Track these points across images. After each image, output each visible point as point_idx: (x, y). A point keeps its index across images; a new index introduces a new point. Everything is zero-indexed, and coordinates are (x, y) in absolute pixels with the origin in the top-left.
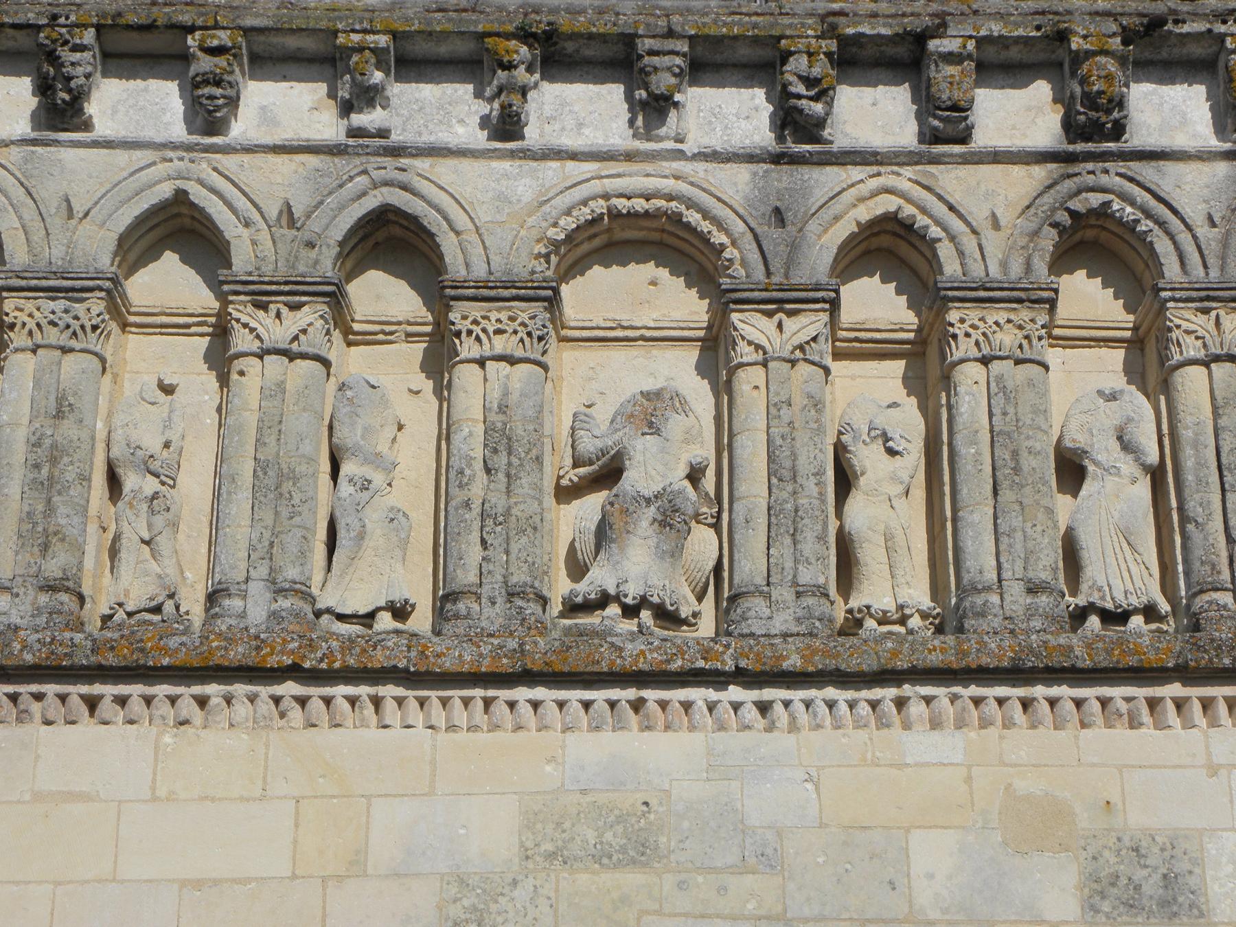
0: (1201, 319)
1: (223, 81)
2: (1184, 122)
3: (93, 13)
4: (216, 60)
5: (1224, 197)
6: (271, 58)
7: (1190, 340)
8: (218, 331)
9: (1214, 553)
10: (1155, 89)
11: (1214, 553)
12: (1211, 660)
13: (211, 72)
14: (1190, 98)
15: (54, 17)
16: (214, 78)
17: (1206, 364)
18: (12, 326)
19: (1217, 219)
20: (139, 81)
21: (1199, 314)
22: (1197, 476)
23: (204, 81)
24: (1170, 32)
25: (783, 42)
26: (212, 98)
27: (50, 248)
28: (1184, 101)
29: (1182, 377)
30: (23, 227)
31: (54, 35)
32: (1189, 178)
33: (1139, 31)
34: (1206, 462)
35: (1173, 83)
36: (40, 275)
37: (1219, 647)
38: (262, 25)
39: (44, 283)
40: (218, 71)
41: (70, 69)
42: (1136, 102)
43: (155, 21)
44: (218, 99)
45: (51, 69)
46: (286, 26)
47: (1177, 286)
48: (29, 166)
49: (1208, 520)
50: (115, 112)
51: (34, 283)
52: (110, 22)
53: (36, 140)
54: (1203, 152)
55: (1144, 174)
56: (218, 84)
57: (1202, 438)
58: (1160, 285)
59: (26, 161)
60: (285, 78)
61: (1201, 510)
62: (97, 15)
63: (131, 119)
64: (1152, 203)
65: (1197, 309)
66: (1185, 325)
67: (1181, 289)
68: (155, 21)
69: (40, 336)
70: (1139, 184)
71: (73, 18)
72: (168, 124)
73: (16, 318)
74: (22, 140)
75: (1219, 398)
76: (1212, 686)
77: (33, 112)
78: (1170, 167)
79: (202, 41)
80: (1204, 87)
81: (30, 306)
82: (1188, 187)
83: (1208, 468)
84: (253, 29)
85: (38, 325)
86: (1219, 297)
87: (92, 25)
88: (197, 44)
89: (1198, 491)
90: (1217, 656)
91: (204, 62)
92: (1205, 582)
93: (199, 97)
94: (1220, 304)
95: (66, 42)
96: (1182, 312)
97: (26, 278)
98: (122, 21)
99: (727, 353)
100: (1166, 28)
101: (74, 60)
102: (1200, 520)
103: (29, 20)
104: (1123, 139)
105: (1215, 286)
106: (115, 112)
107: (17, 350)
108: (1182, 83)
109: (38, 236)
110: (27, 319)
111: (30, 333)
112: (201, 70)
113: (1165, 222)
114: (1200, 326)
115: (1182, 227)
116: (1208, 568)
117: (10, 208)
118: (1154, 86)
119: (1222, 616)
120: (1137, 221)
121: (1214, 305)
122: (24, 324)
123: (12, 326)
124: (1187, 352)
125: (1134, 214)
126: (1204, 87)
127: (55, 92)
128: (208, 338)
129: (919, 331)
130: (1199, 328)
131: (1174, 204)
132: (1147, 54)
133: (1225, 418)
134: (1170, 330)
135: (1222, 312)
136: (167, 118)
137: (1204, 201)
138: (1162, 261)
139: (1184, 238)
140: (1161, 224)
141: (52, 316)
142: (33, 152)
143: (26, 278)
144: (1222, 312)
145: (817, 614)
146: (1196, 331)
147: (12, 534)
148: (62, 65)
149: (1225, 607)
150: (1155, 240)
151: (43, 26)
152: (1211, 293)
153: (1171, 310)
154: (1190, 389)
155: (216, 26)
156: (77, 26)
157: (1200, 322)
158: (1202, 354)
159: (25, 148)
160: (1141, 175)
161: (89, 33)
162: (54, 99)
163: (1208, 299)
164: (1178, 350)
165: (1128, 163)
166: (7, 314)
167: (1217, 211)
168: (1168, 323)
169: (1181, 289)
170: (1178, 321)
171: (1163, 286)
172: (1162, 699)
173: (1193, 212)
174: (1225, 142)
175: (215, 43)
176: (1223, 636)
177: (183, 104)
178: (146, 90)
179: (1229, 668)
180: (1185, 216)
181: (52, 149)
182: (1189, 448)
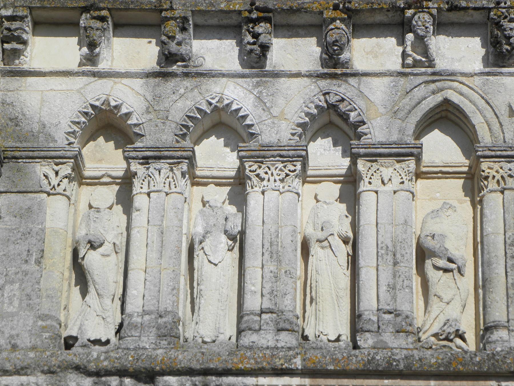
8: (237, 181)
10: (378, 45)
18: (486, 178)
25: (164, 12)
27: (503, 133)
30: (487, 122)
31: (499, 13)
36: (502, 149)
39: (505, 153)
41: (509, 32)
48: (486, 88)
51: (499, 153)
53: (489, 72)
59: (484, 85)
69: (503, 183)
73: (489, 173)
74: (481, 73)
77: (483, 57)
81: (496, 166)
85: (502, 177)
95: (506, 17)
97: (494, 151)
99: (478, 183)
103: (484, 5)
107: (491, 191)
109: (496, 127)
110: (495, 174)
111: (498, 182)
117: (477, 111)
122: (494, 177)
123: (486, 178)
128: (229, 188)
129: (470, 167)
141: (510, 172)
142: (487, 79)
143: (494, 151)
145: (402, 6)
147: (504, 296)
148: (505, 30)
151: (492, 8)
159: (483, 77)
162: (501, 49)
166: (483, 171)
181: (498, 77)
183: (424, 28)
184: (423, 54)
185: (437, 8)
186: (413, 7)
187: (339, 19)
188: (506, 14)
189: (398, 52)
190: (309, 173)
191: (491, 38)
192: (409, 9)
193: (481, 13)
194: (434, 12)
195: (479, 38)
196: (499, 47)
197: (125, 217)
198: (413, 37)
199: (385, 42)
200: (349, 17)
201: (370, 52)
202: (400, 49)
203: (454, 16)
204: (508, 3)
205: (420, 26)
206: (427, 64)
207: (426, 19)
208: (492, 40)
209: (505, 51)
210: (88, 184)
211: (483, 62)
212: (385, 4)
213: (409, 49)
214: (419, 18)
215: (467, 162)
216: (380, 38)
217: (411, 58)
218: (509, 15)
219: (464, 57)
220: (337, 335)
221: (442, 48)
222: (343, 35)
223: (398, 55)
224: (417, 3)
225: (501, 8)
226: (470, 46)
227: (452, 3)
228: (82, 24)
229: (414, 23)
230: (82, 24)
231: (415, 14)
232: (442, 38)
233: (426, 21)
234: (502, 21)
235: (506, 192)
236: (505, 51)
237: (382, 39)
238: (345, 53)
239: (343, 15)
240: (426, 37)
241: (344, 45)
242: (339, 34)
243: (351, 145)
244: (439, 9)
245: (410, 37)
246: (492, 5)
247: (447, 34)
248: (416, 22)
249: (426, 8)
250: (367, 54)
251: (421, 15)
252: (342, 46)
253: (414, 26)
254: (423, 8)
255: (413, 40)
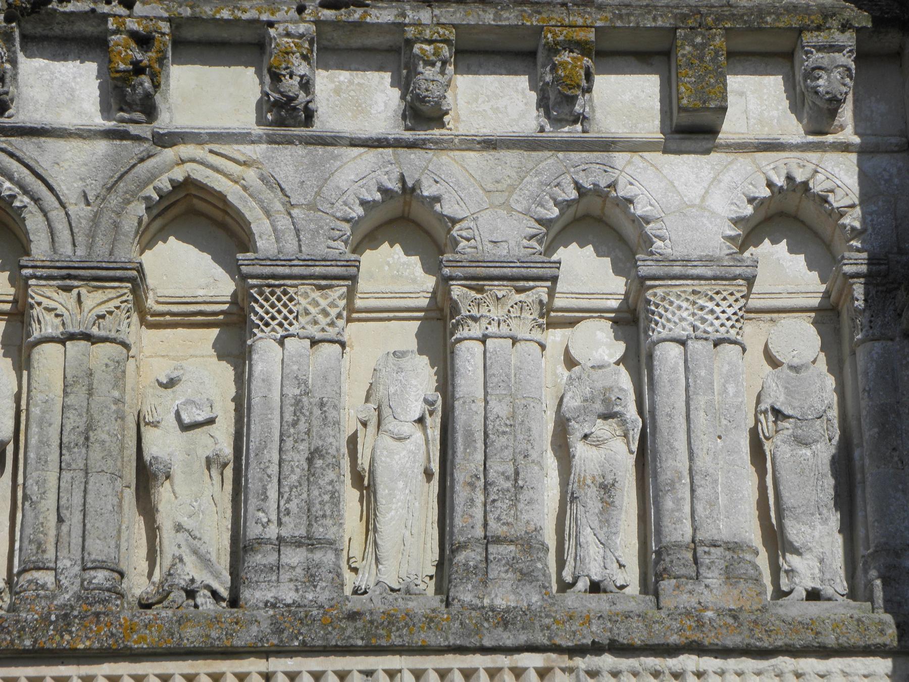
0: (63, 296)
2: (72, 99)
5: (101, 175)
7: (49, 317)
9: (42, 532)
10: (46, 65)
11: (42, 532)
12: (12, 641)
14: (81, 75)
17: (63, 342)
19: (91, 198)
21: (60, 292)
22: (38, 454)
24: (55, 10)
28: (75, 78)
29: (39, 354)
32: (69, 155)
33: (26, 8)
34: (48, 440)
35: (66, 60)
37: (23, 628)
42: (26, 78)
47: (39, 264)
49: (41, 498)
54: (83, 130)
55: (24, 150)
57: (48, 416)
58: (22, 263)
61: (36, 488)
64: (29, 178)
65: (59, 287)
66: (46, 302)
67: (43, 267)
70: (19, 160)
75: (69, 377)
76: (16, 666)
78: (50, 144)
80: (96, 64)
82: (66, 165)
83: (48, 445)
86: (79, 275)
89: (37, 469)
90: (19, 637)
92: (29, 561)
94: (82, 283)
96: (44, 289)
100: (50, 6)
102: (34, 498)
104: (7, 114)
105: (76, 265)
108: (74, 60)
113: (39, 199)
114: (61, 304)
115: (57, 204)
116: (34, 547)
118: (46, 61)
119: (38, 595)
120: (13, 197)
121: (76, 283)
124: (46, 330)
125: (10, 189)
126: (96, 64)
130: (59, 306)
131: (50, 181)
132: (40, 30)
133: (72, 396)
134: (32, 307)
135: (83, 291)
137: (81, 179)
138: (32, 237)
139: (57, 215)
140: (36, 200)
144: (83, 291)
146: (56, 309)
149: (43, 587)
150: (27, 216)
152: (72, 272)
153: (33, 287)
154: (43, 366)
157: (61, 300)
158: (58, 332)
160: (22, 151)
163: (69, 277)
164: (38, 326)
165: (10, 139)
167: (92, 189)
168: (30, 300)
169: (43, 267)
170: (38, 298)
171: (25, 263)
172: (476, 670)
173: (68, 189)
174: (109, 119)
176: (29, 617)
179: (28, 650)
180: (60, 194)
182: (35, 425)
190: (359, 303)
197: (226, 371)
208: (13, 49)
210: (359, 320)
215: (12, 291)
228: (670, 24)
230: (670, 24)
235: (488, 341)
243: (238, 260)
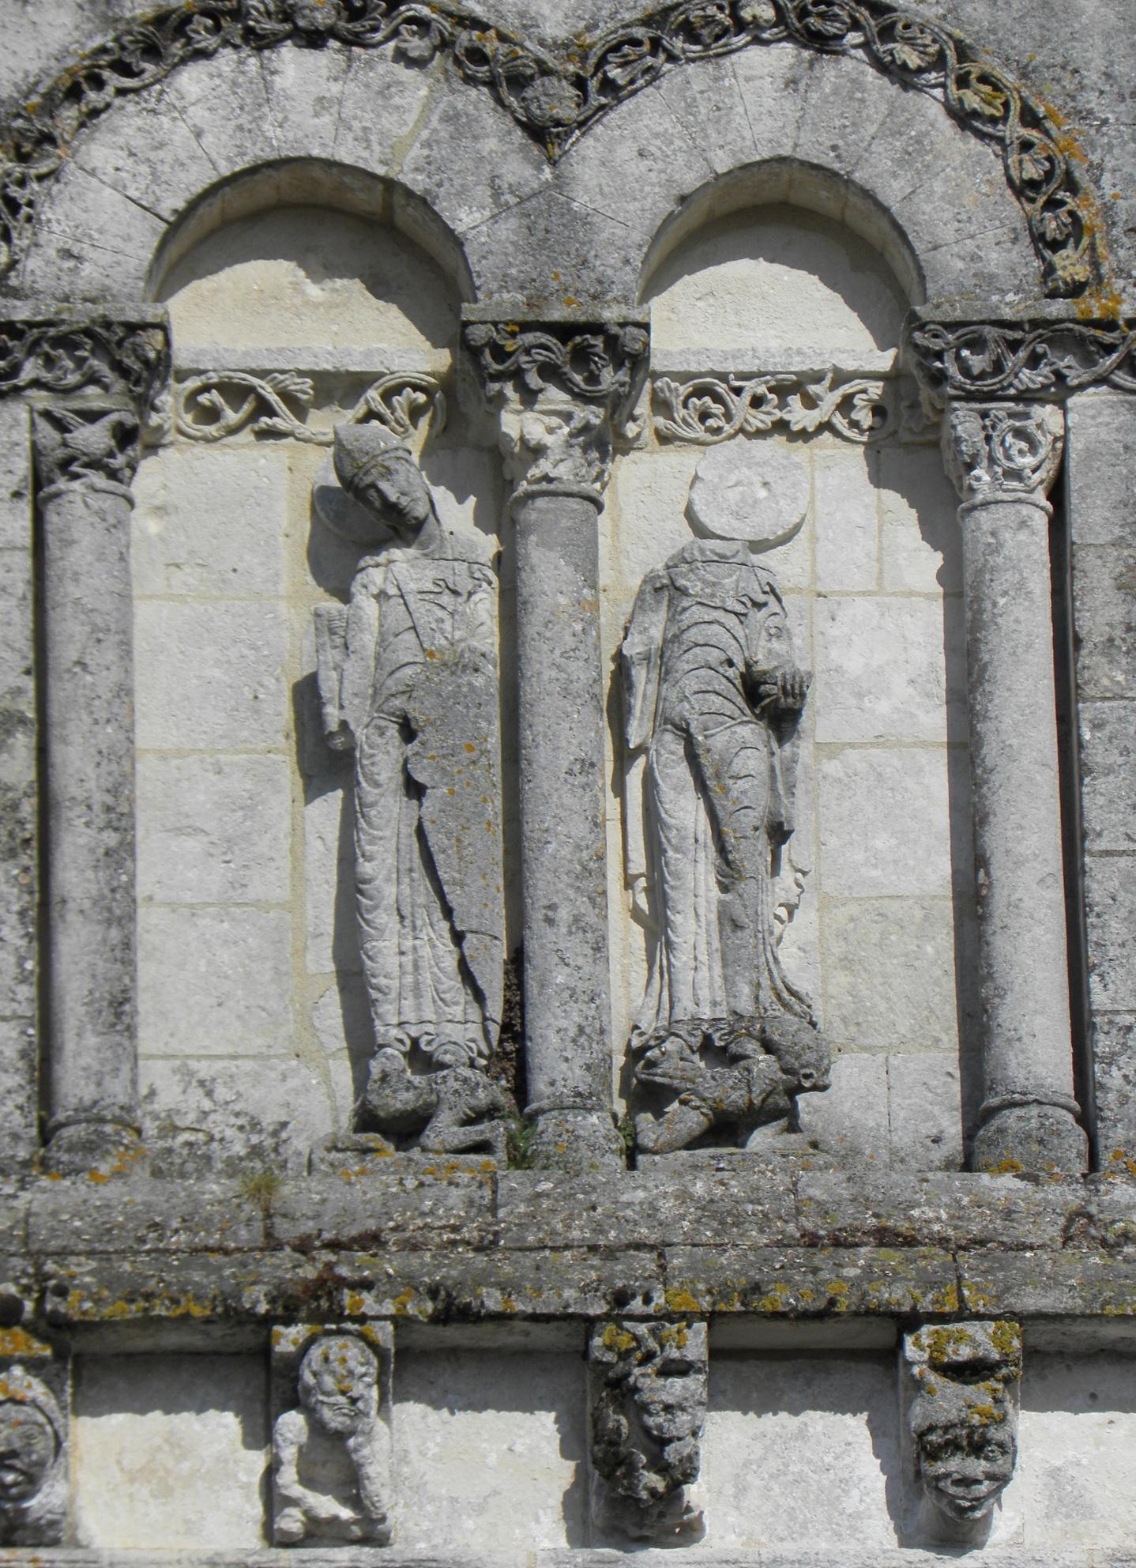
1: (989, 1442)
3: (701, 1286)
4: (969, 1390)
6: (1060, 1354)
10: (172, 1440)
13: (963, 1423)
15: (621, 1298)
16: (970, 1436)
20: (783, 1415)
23: (948, 1443)
26: (967, 1482)
31: (625, 1342)
38: (1060, 1308)
40: (976, 1419)
43: (832, 1302)
44: (979, 1482)
45: (624, 1421)
46: (1111, 1310)
50: (741, 1491)
52: (738, 1307)
56: (977, 1448)
60: (1094, 1402)
62: (709, 1292)
63: (778, 1506)
68: (832, 1302)
71: (659, 1299)
72: (857, 1516)
77: (567, 1494)
79: (936, 1348)
84: (1040, 1316)
87: (702, 1316)
88: (926, 1356)
91: (944, 1397)
93: (938, 1478)
95: (649, 1357)
98: (764, 1304)
101: (671, 1400)
103: (567, 1306)
106: (741, 1491)
112: (942, 1419)
127: (632, 1470)
136: (852, 1502)
145: (263, 1308)
155: (962, 1314)
156: (670, 1317)
161: (697, 1333)
162: (632, 1487)
175: (965, 1353)
177: (883, 1469)
178: (802, 1434)
183: (342, 1400)
184: (345, 1483)
185: (392, 1318)
186: (303, 1314)
187: (21, 1361)
188: (652, 1344)
189: (250, 1472)
191: (597, 1442)
192: (288, 1322)
193: (558, 1329)
194: (384, 1333)
195: (553, 1415)
196: (625, 1476)
198: (306, 1430)
199: (197, 1427)
200: (60, 1355)
201: (141, 1470)
202: (258, 1460)
203: (455, 1334)
204: (659, 1299)
205: (328, 1394)
206: (357, 1531)
207: (352, 1364)
209: (644, 1495)
211: (566, 1518)
212: (198, 1298)
213: (288, 1478)
214: (326, 1359)
216: (178, 1412)
217: (296, 1512)
218: (662, 1347)
219: (496, 1493)
220: (284, 712)
221: (414, 1456)
222: (35, 1430)
223: (248, 1485)
224: (318, 1298)
225: (631, 1317)
226: (519, 1448)
227: (449, 1295)
229: (308, 1378)
231: (311, 1341)
232: (411, 1413)
233: (351, 1373)
234: (637, 1371)
236: (644, 1495)
237: (187, 1417)
238: (45, 1489)
239: (36, 1345)
240: (353, 1433)
241: (41, 1464)
242: (20, 1423)
244: (401, 1322)
245: (292, 1424)
246: (598, 1308)
247: (434, 1394)
248: (315, 1374)
249: (354, 1319)
250: (132, 1481)
251: (334, 1345)
252: (33, 1470)
253: (308, 1391)
254: (340, 1318)
255: (304, 1438)
